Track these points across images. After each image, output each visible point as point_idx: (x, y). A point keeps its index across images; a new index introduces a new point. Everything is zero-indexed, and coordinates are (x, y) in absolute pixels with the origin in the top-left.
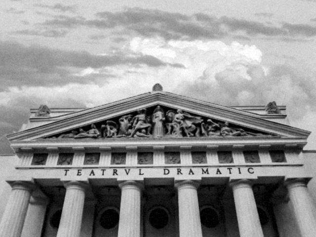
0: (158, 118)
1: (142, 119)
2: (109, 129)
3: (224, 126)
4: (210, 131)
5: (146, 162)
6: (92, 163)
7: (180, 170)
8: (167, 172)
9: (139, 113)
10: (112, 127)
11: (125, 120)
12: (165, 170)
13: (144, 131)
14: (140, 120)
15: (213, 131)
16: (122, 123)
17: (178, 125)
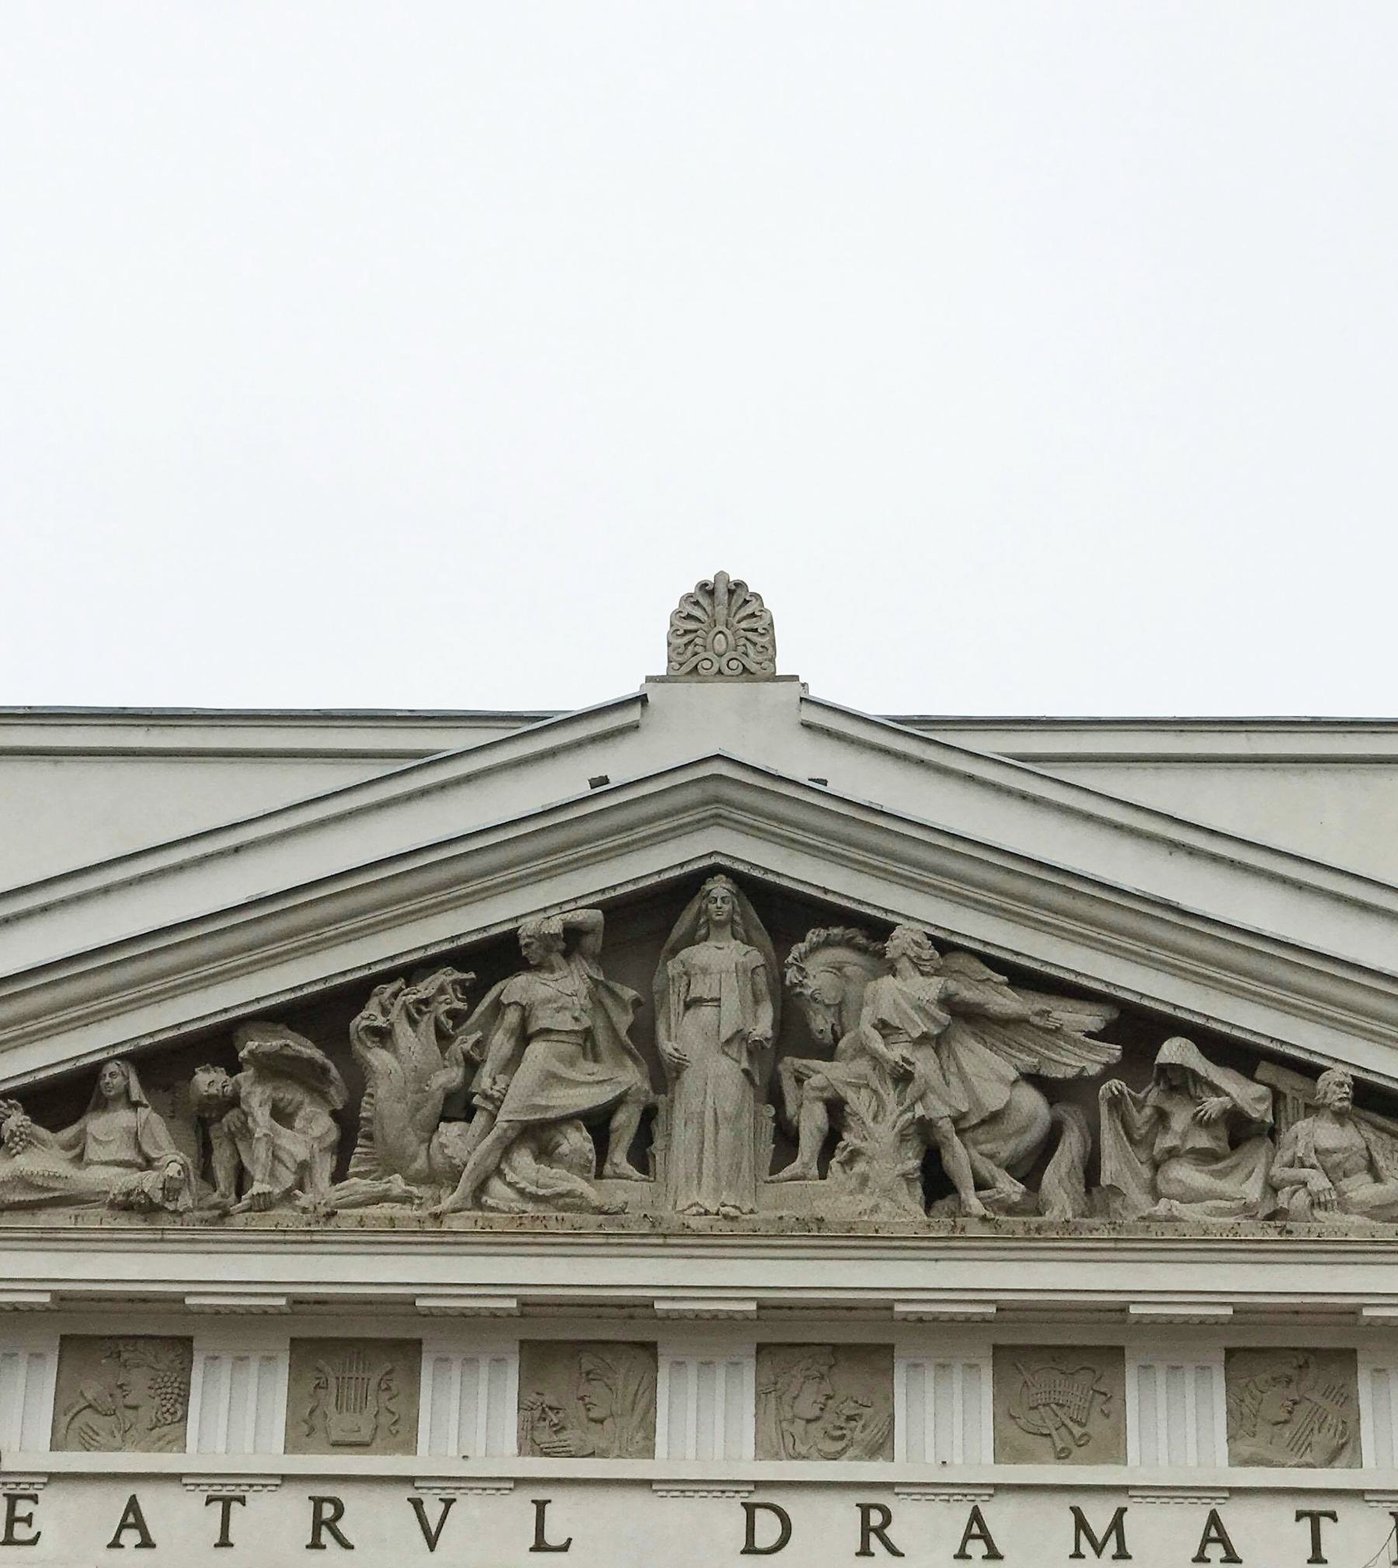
0: (707, 1012)
1: (565, 1022)
2: (261, 1118)
3: (1312, 1109)
4: (1172, 1153)
5: (596, 1438)
6: (124, 1439)
7: (887, 1519)
8: (768, 1529)
9: (534, 955)
10: (292, 1094)
11: (403, 1032)
12: (750, 1509)
13: (577, 1141)
14: (546, 1032)
15: (1204, 1157)
16: (378, 1058)
17: (890, 1095)
